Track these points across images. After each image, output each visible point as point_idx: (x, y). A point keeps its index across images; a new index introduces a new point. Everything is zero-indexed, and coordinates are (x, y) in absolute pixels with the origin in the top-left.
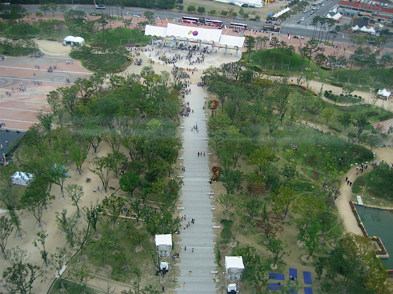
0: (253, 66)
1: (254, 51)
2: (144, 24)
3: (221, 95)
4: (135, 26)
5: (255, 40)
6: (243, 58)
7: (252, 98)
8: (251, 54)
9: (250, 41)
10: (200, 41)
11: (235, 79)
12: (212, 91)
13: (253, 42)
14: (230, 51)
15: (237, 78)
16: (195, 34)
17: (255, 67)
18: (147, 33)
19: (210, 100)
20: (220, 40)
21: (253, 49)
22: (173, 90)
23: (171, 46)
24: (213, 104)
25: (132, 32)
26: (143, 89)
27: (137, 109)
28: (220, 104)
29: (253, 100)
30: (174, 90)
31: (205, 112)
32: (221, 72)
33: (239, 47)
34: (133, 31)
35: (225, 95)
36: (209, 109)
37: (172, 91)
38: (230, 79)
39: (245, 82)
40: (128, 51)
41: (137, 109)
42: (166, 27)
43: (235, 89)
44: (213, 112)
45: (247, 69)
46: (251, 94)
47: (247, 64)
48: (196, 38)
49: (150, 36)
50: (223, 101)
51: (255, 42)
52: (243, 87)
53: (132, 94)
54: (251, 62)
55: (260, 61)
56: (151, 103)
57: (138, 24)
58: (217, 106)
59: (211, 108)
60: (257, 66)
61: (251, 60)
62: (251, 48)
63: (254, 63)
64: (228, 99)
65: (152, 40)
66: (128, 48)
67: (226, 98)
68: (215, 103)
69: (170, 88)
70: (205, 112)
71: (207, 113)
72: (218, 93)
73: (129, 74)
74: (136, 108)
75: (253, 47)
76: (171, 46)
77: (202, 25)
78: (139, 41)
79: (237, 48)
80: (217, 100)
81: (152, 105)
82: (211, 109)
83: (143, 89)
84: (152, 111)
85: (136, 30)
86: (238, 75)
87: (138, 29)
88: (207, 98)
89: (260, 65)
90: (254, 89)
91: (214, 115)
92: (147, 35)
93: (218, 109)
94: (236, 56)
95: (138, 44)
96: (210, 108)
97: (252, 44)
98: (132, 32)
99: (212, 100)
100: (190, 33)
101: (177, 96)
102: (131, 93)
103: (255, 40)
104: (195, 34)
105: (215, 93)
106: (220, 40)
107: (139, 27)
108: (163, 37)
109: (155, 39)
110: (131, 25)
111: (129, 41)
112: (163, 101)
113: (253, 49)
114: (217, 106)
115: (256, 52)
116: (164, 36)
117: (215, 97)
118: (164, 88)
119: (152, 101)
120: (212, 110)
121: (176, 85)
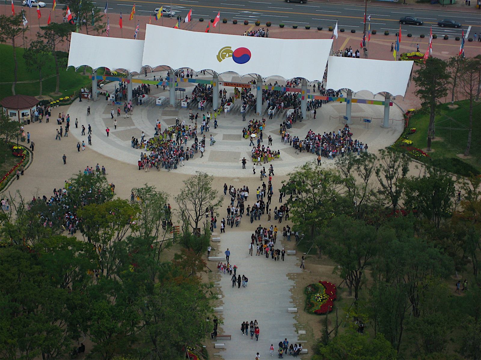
0: (449, 156)
1: (445, 107)
2: (64, 30)
3: (349, 265)
4: (35, 39)
5: (449, 70)
6: (407, 132)
7: (458, 269)
8: (437, 118)
9: (429, 76)
10: (349, 92)
11: (390, 205)
12: (313, 252)
13: (441, 77)
14: (361, 110)
15: (395, 202)
16: (242, 56)
17: (457, 161)
18: (75, 60)
19: (309, 282)
20: (326, 74)
21: (442, 100)
22: (179, 253)
23: (158, 102)
24: (320, 297)
25: (24, 56)
26: (77, 254)
27: (57, 324)
28: (344, 295)
29: (459, 277)
30: (183, 251)
31: (295, 325)
32: (341, 182)
33: (394, 94)
34: (29, 55)
35: (362, 262)
36: (311, 313)
37: (177, 256)
38: (372, 207)
39: (428, 215)
40: (14, 122)
41: (61, 325)
42: (142, 37)
43: (395, 241)
44: (325, 323)
45: (428, 168)
46: (452, 255)
47: (425, 150)
48: (243, 70)
49: (85, 69)
50: (356, 284)
51: (447, 77)
52: (422, 231)
53: (41, 273)
54: (437, 143)
55: (470, 140)
56: (109, 302)
57: (43, 32)
58: (336, 303)
59: (317, 308)
60: (461, 156)
61: (437, 139)
62: (434, 97)
63: (449, 146)
64: (373, 275)
65: (94, 84)
66: (10, 111)
67: (367, 272)
68: (327, 293)
69: (169, 245)
70: (295, 325)
71: (304, 328)
72: (333, 256)
73: (22, 204)
74: (56, 320)
75: (443, 92)
76: (158, 102)
77: (446, 38)
78: (49, 87)
79: (388, 100)
80: (336, 280)
81: (111, 309)
82: (316, 313)
83: (77, 254)
84: (111, 331)
85: (38, 51)
86: (398, 193)
87: (43, 48)
88: (298, 274)
89: (471, 153)
90: (460, 236)
91: (332, 335)
92: (77, 65)
93: (341, 312)
94: (382, 127)
95: (47, 98)
96: (313, 310)
97: (439, 84)
98: (24, 56)
99: (315, 280)
100: (224, 57)
101: (194, 272)
102: (37, 268)
103: (449, 70)
104: (242, 56)
105: (326, 257)
106: (326, 74)
107: (46, 41)
108: (131, 71)
109: (104, 78)
110: (21, 34)
111: (13, 90)
112: (150, 290)
113: (442, 100)
114: (336, 303)
115: (452, 110)
116: (133, 67)
117: (325, 271)
118: (145, 244)
119: (112, 294)
120: (323, 317)
121: (187, 234)
